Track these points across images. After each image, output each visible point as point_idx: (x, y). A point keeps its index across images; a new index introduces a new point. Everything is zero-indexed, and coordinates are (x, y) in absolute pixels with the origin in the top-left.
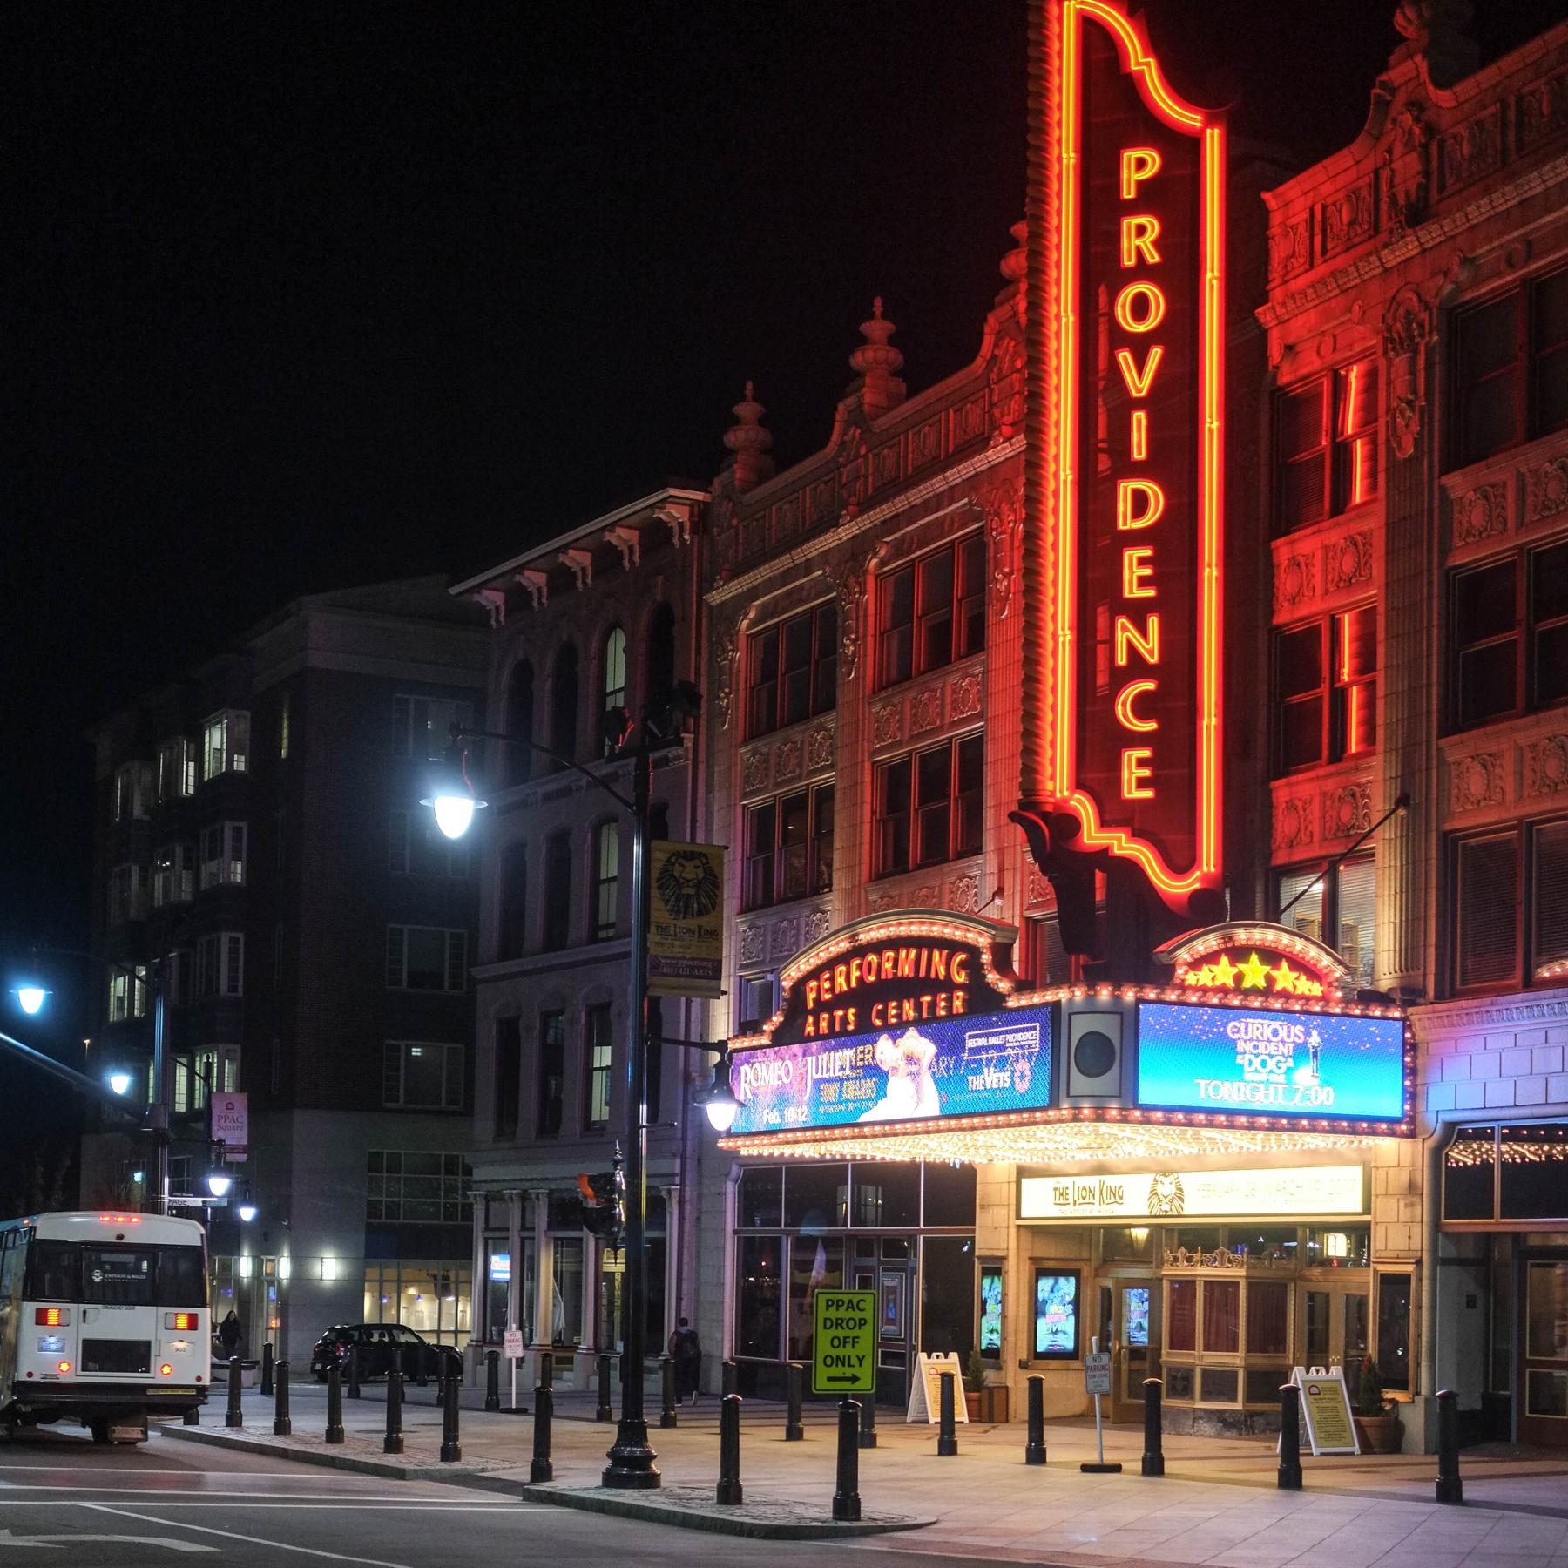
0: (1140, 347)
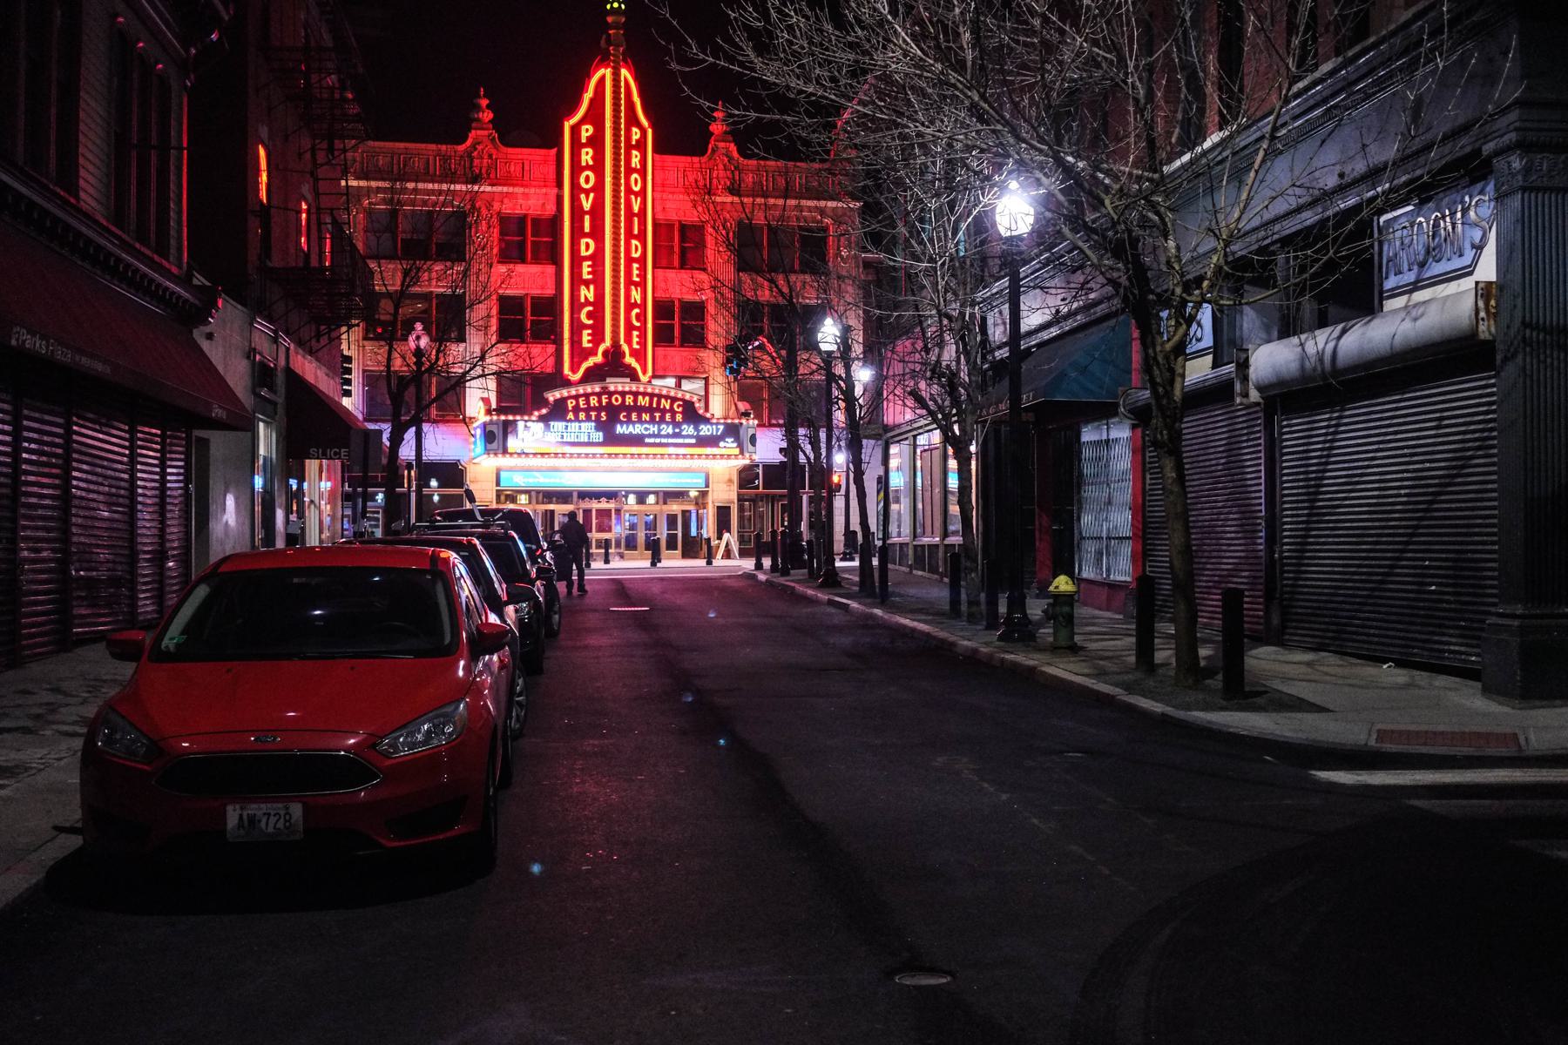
0: (587, 192)
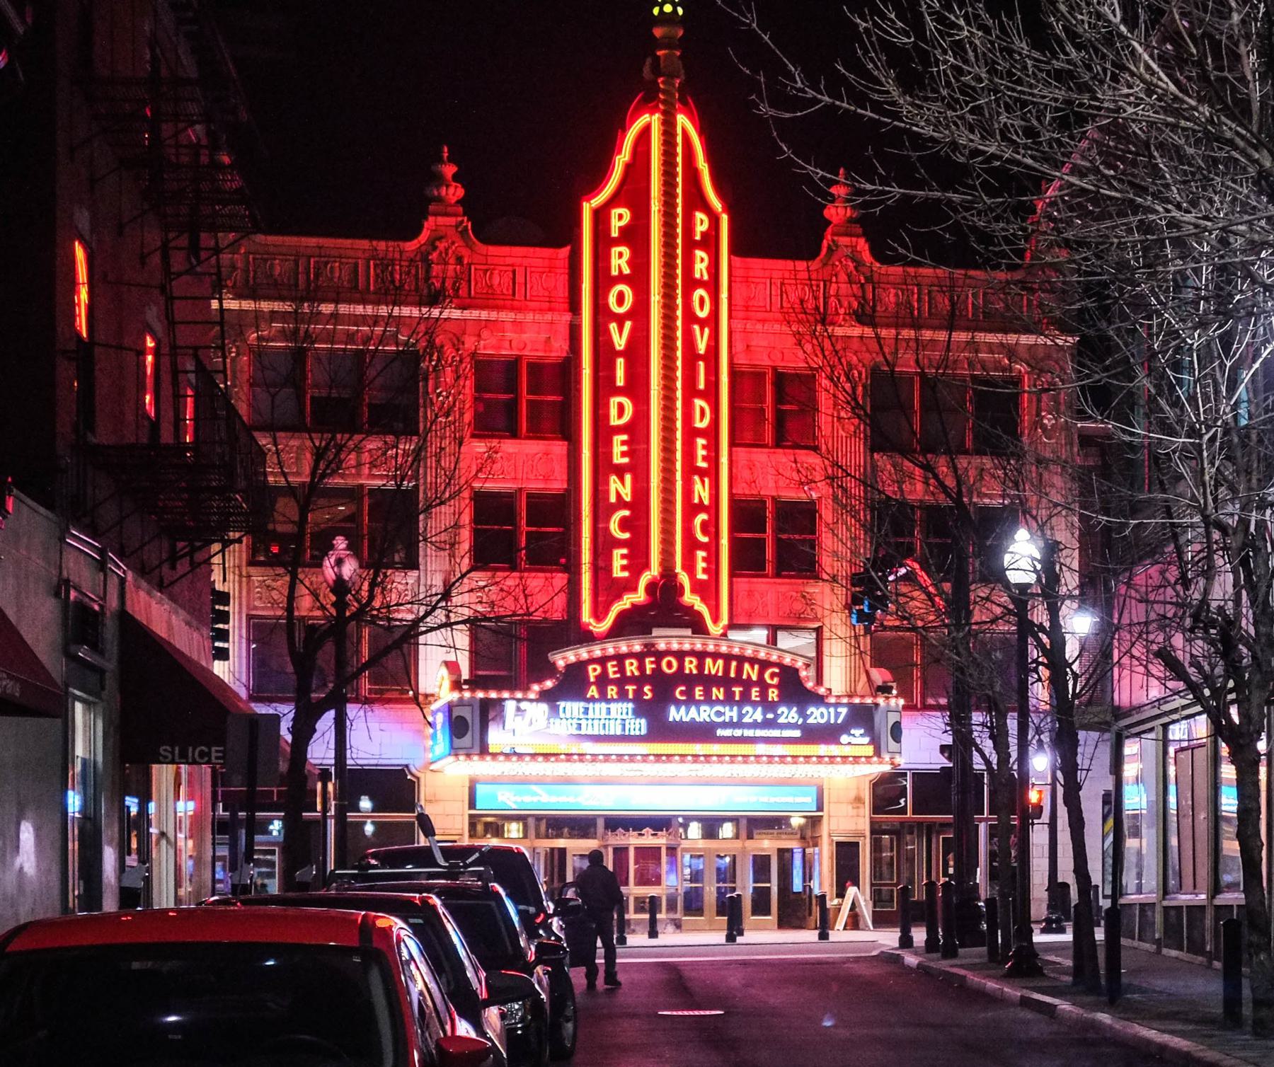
0: (620, 319)
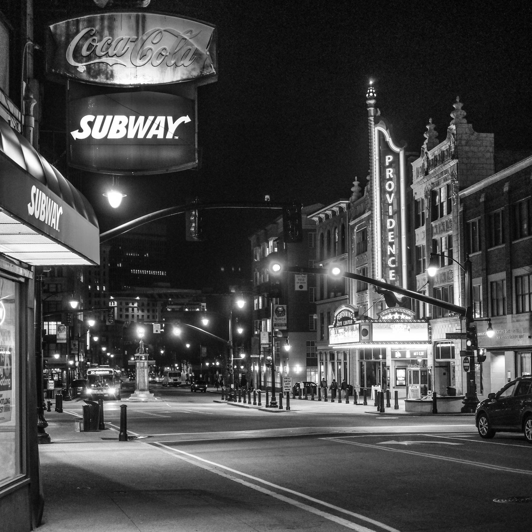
0: (390, 193)
